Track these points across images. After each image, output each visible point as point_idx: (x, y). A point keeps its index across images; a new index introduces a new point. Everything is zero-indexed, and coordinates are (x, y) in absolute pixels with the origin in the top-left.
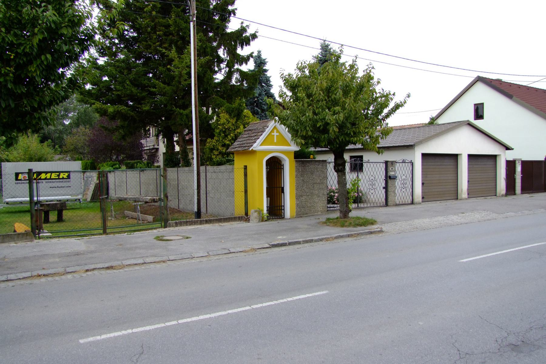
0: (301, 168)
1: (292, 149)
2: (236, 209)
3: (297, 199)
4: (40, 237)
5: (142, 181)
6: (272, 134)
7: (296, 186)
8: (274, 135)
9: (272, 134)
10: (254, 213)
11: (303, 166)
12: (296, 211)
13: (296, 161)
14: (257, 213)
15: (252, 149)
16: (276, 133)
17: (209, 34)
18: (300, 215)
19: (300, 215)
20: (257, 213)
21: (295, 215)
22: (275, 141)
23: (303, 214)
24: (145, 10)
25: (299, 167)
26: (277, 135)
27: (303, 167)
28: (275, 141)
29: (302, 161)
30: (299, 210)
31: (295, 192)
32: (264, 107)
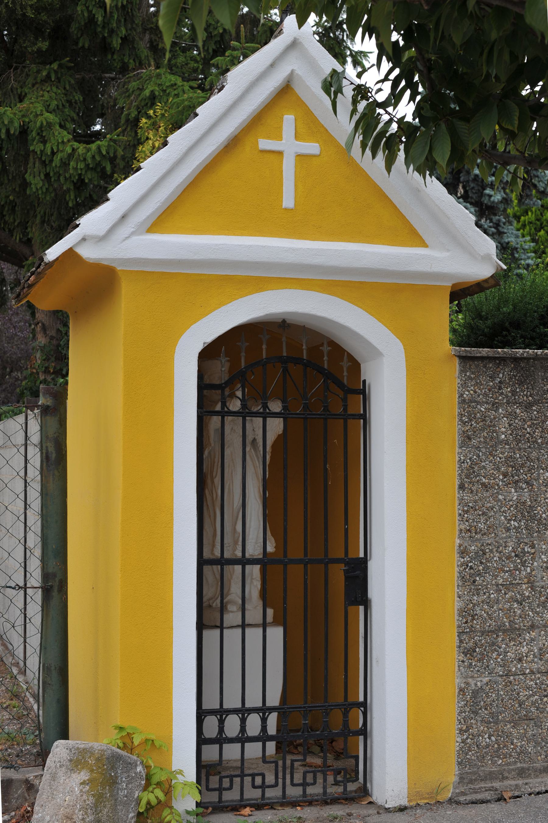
0: (512, 415)
1: (437, 268)
2: (103, 748)
3: (468, 652)
4: (267, 760)
5: (218, 615)
6: (265, 144)
7: (463, 552)
8: (280, 153)
9: (265, 144)
10: (61, 773)
11: (524, 396)
12: (464, 751)
13: (463, 359)
14: (84, 775)
15: (70, 253)
16: (297, 137)
17: (403, 46)
18: (491, 776)
19: (491, 776)
20: (84, 775)
21: (453, 778)
22: (288, 201)
23: (522, 773)
24: (242, 26)
25: (495, 406)
26: (301, 157)
27: (528, 407)
28: (288, 201)
29: (516, 360)
30: (485, 740)
31: (457, 604)
32: (490, 196)
